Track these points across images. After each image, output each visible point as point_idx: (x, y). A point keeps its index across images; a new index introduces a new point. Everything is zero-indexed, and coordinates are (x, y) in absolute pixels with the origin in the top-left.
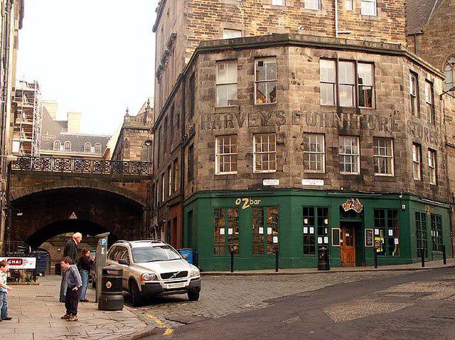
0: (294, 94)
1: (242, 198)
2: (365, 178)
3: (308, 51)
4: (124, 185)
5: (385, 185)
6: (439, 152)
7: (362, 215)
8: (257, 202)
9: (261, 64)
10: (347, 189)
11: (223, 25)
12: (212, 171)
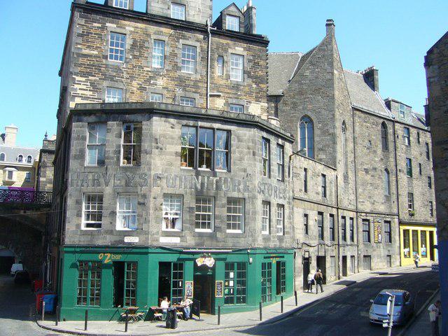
1: (104, 253)
2: (219, 235)
3: (172, 120)
4: (25, 212)
6: (286, 206)
7: (213, 268)
10: (198, 245)
11: (105, 84)
12: (78, 226)
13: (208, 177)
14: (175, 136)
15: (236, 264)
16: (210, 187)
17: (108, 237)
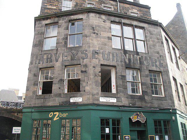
0: (94, 40)
1: (54, 112)
2: (146, 97)
3: (103, 17)
4: (17, 114)
5: (160, 103)
8: (65, 115)
9: (73, 24)
13: (133, 55)
14: (106, 27)
15: (162, 122)
16: (135, 62)
17: (57, 99)
